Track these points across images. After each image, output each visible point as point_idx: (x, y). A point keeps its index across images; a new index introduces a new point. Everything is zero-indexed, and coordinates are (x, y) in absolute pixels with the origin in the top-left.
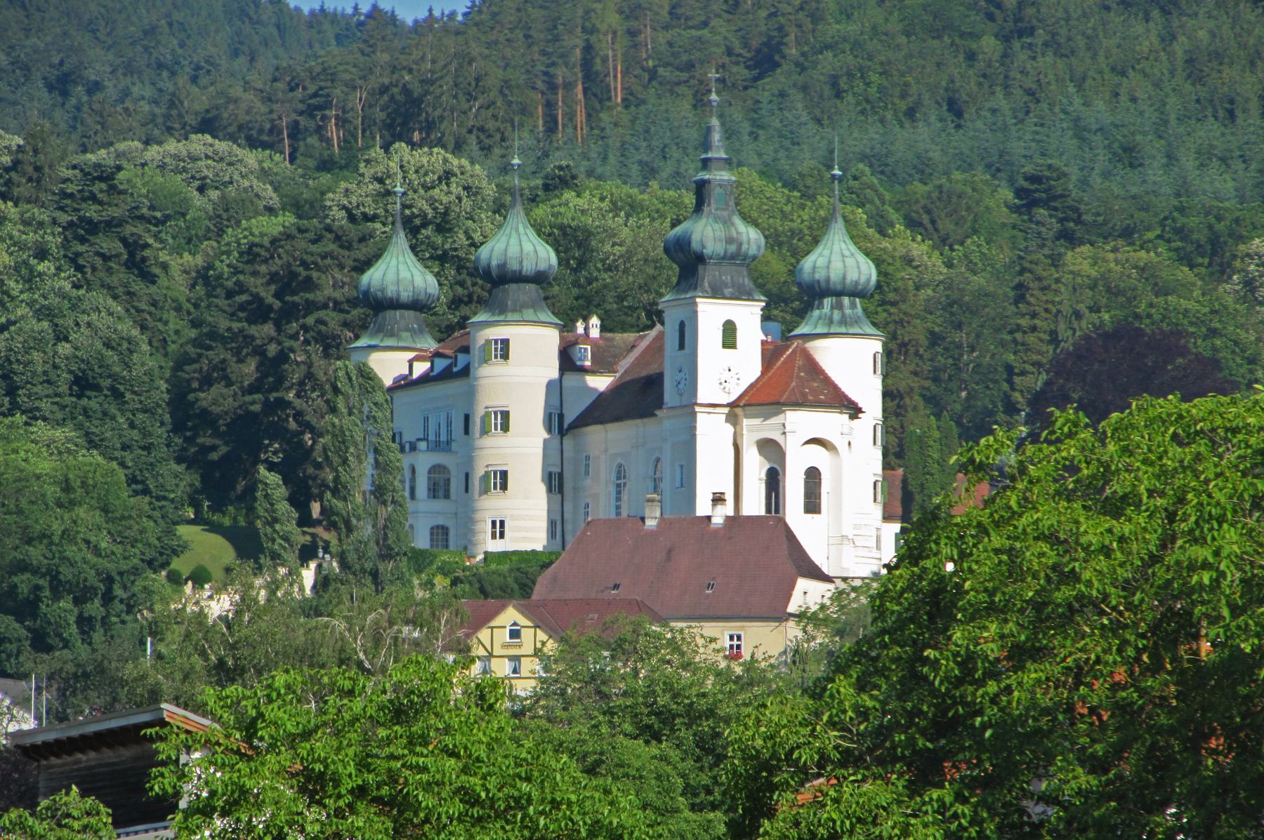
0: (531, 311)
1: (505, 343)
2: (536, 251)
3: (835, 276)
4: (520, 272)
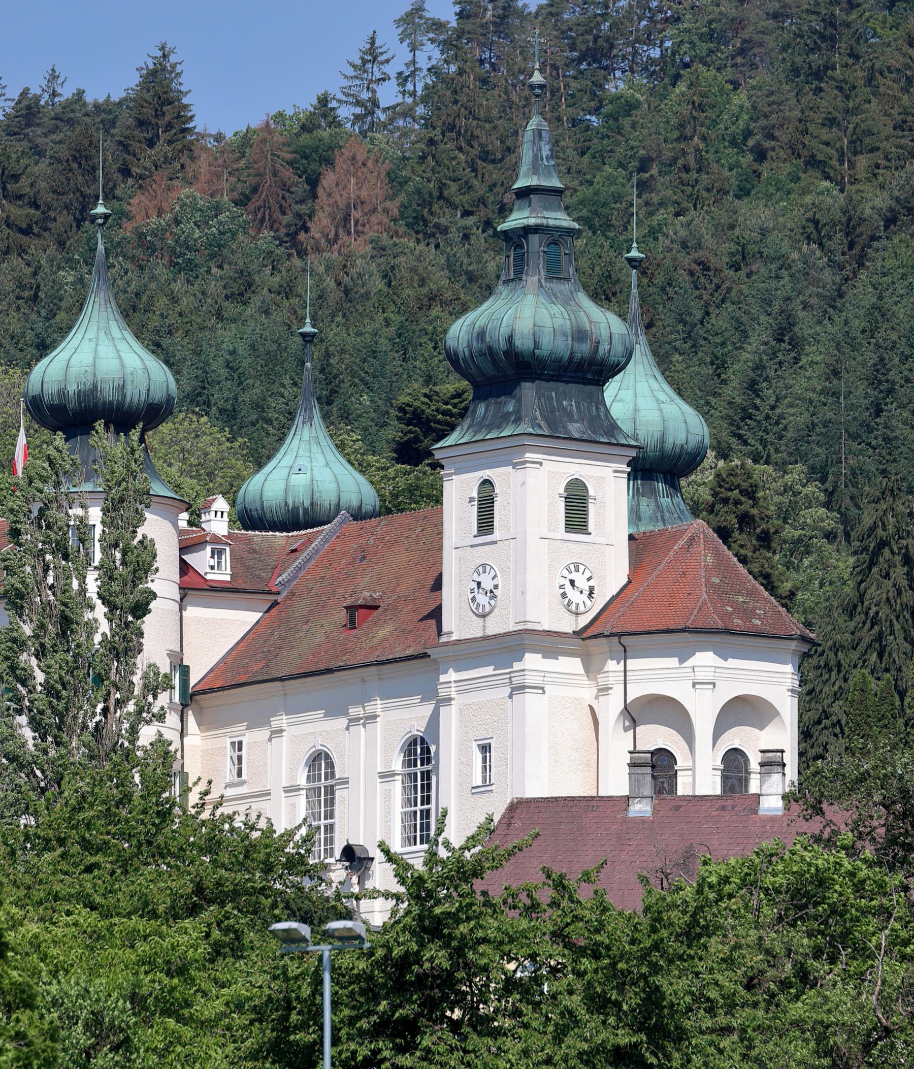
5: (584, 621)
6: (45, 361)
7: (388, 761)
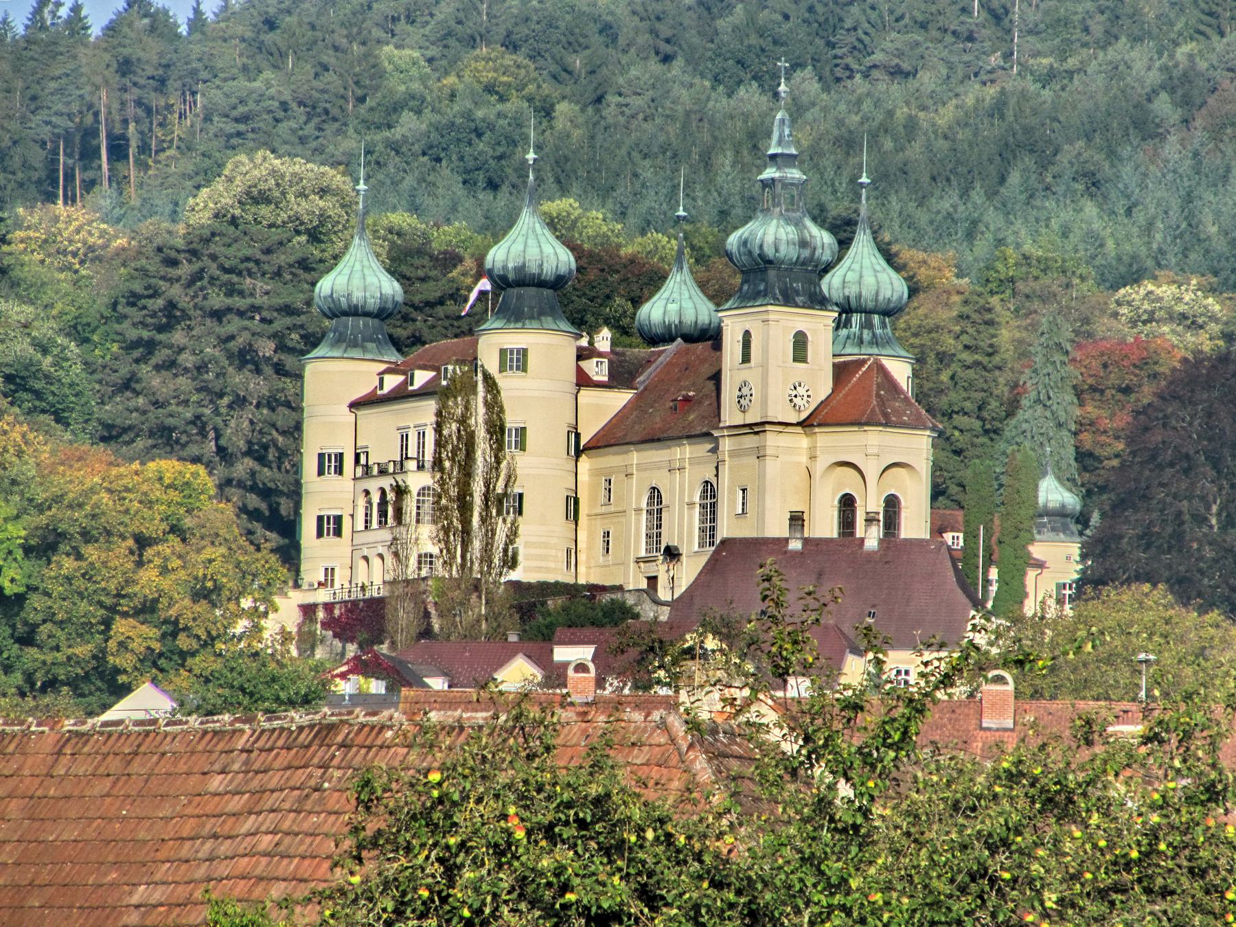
0: (550, 319)
2: (556, 253)
3: (867, 293)
4: (540, 275)
5: (804, 415)
6: (495, 248)
7: (691, 496)
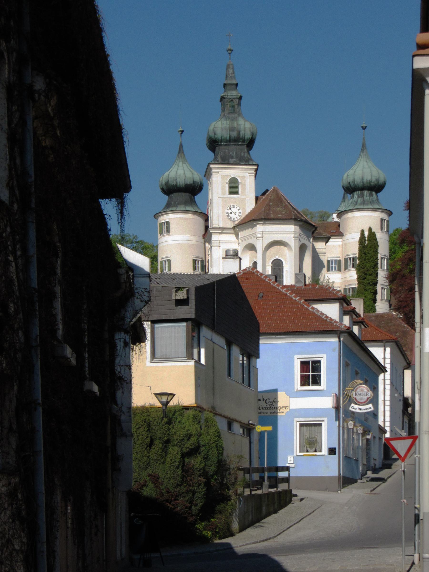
1: (168, 223)
